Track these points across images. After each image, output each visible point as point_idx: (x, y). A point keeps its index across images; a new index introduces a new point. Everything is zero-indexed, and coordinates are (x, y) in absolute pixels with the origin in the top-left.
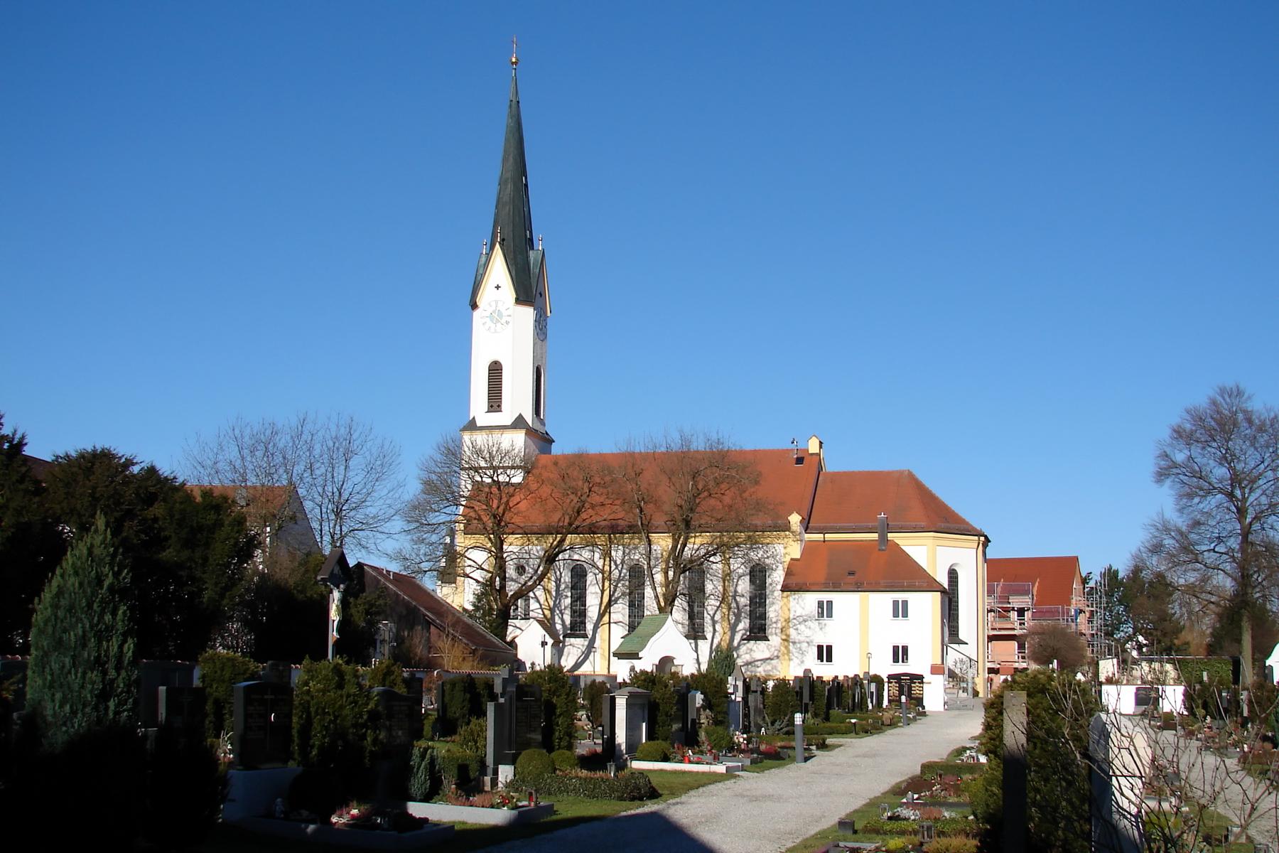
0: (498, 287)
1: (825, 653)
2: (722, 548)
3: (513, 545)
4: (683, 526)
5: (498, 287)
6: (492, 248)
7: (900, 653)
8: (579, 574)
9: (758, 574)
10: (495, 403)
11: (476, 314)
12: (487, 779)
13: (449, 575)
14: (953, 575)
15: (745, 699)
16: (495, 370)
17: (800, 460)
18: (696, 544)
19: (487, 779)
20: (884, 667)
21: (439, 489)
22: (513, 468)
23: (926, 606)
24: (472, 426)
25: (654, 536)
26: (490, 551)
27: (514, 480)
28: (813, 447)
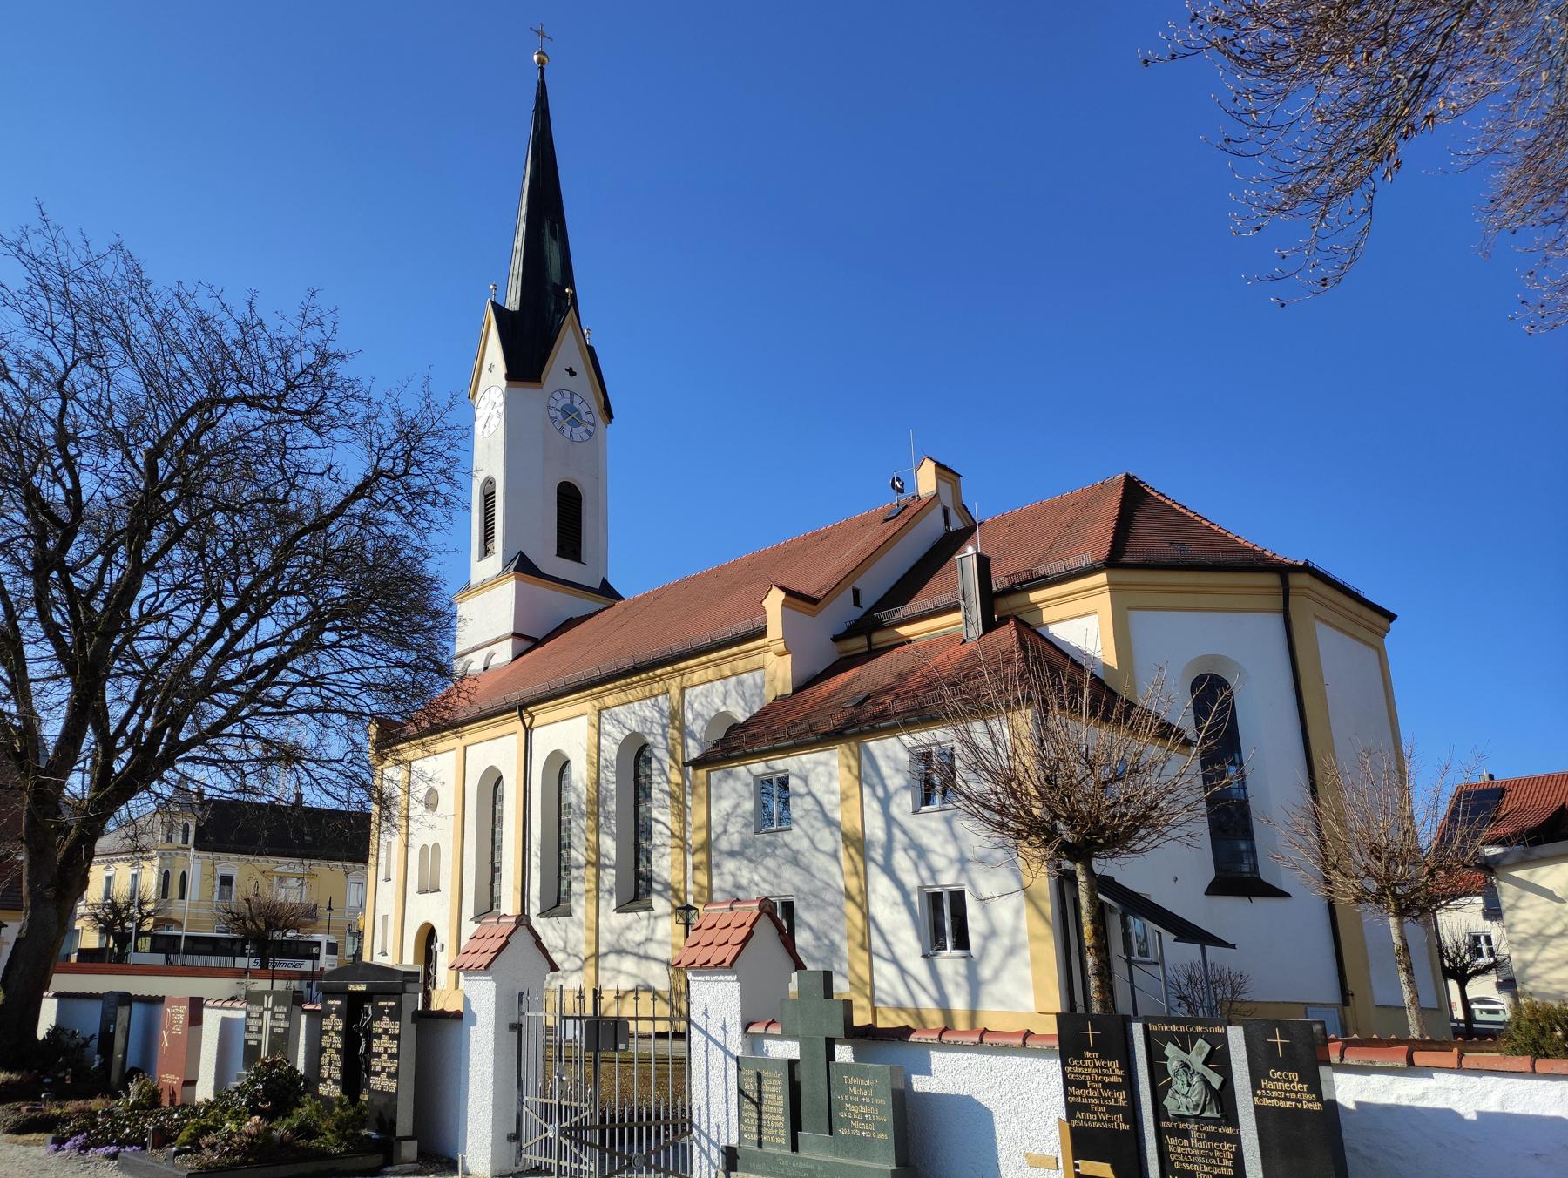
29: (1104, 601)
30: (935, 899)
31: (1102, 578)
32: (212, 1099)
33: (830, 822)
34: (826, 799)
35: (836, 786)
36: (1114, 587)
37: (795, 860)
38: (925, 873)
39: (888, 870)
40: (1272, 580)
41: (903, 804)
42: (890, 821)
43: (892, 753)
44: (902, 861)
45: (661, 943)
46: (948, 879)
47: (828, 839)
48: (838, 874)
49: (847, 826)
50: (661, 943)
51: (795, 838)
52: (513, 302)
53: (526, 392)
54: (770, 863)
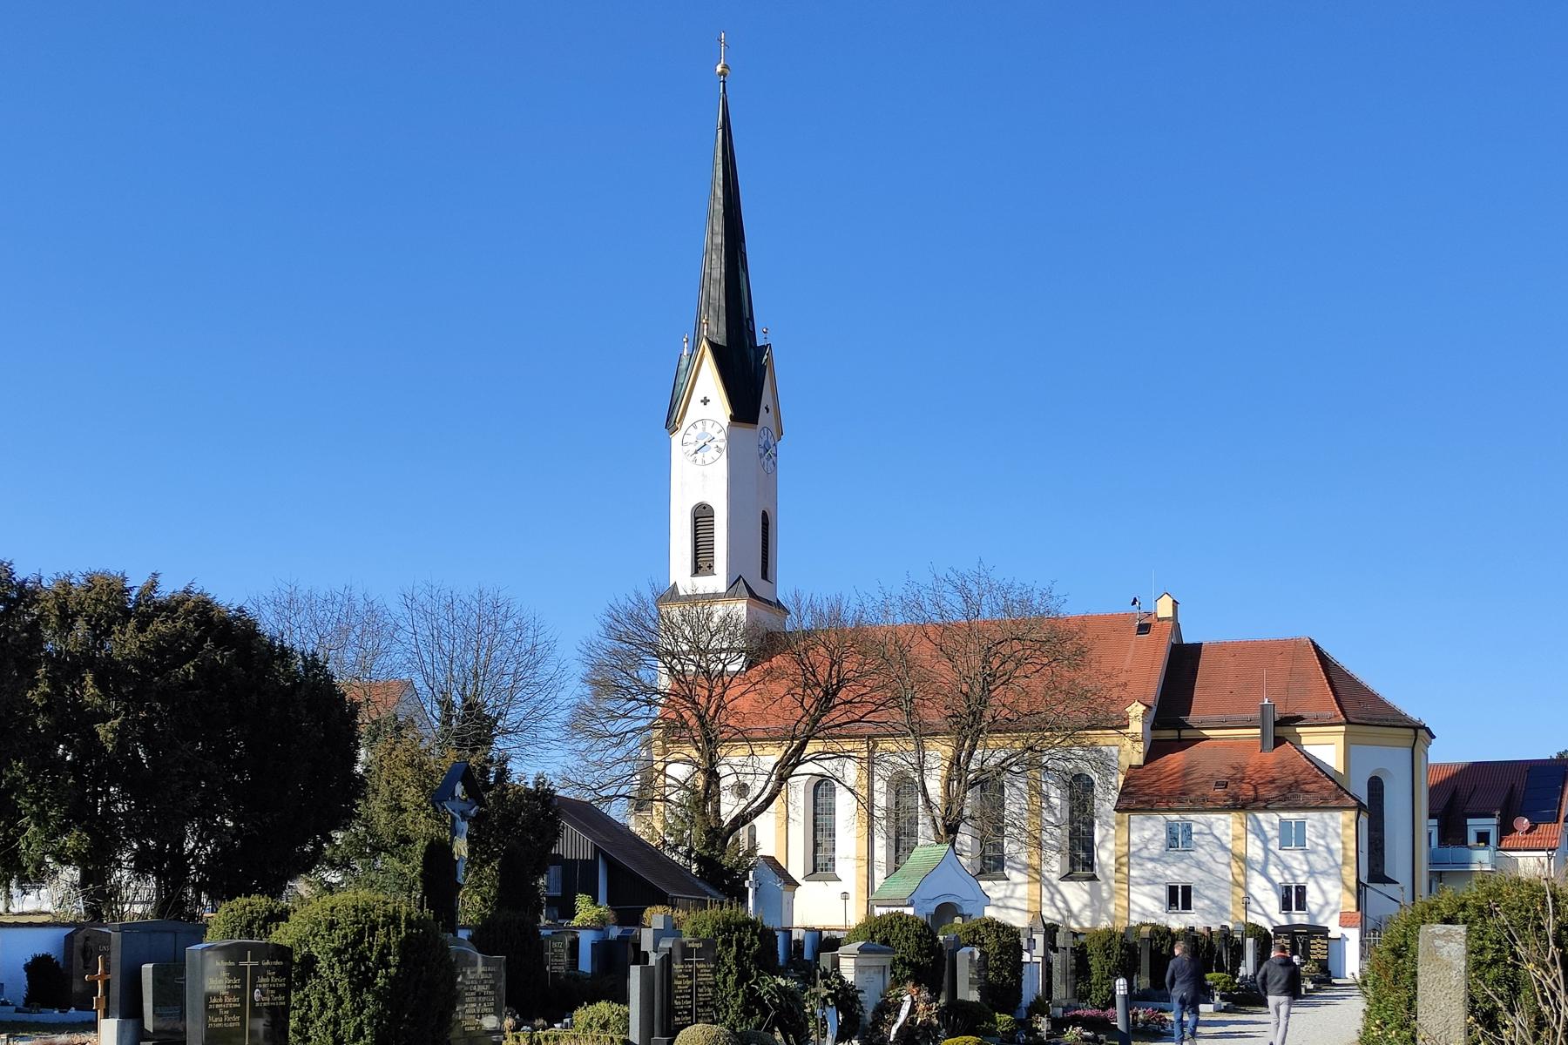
0: (705, 401)
1: (1180, 897)
2: (1031, 760)
3: (732, 762)
4: (969, 725)
5: (705, 401)
6: (696, 345)
7: (1292, 897)
8: (822, 788)
9: (1080, 791)
10: (701, 563)
11: (676, 439)
12: (881, 800)
13: (641, 804)
14: (1376, 786)
15: (1046, 958)
16: (702, 516)
17: (1144, 628)
18: (992, 752)
19: (881, 800)
20: (1269, 913)
21: (614, 681)
22: (729, 650)
23: (1336, 831)
24: (672, 594)
25: (928, 743)
26: (697, 765)
27: (730, 668)
28: (1164, 609)
29: (1341, 738)
30: (1288, 889)
31: (1343, 728)
32: (1367, 1008)
33: (1223, 847)
34: (1224, 839)
35: (1230, 832)
36: (1346, 734)
37: (1199, 865)
38: (1287, 876)
39: (1264, 873)
40: (1411, 732)
41: (1274, 846)
42: (1266, 850)
43: (1269, 820)
44: (1273, 871)
45: (1019, 899)
46: (1301, 880)
47: (1223, 857)
48: (1225, 869)
49: (1236, 851)
50: (1019, 899)
51: (1201, 854)
52: (721, 340)
53: (745, 431)
54: (1182, 865)
